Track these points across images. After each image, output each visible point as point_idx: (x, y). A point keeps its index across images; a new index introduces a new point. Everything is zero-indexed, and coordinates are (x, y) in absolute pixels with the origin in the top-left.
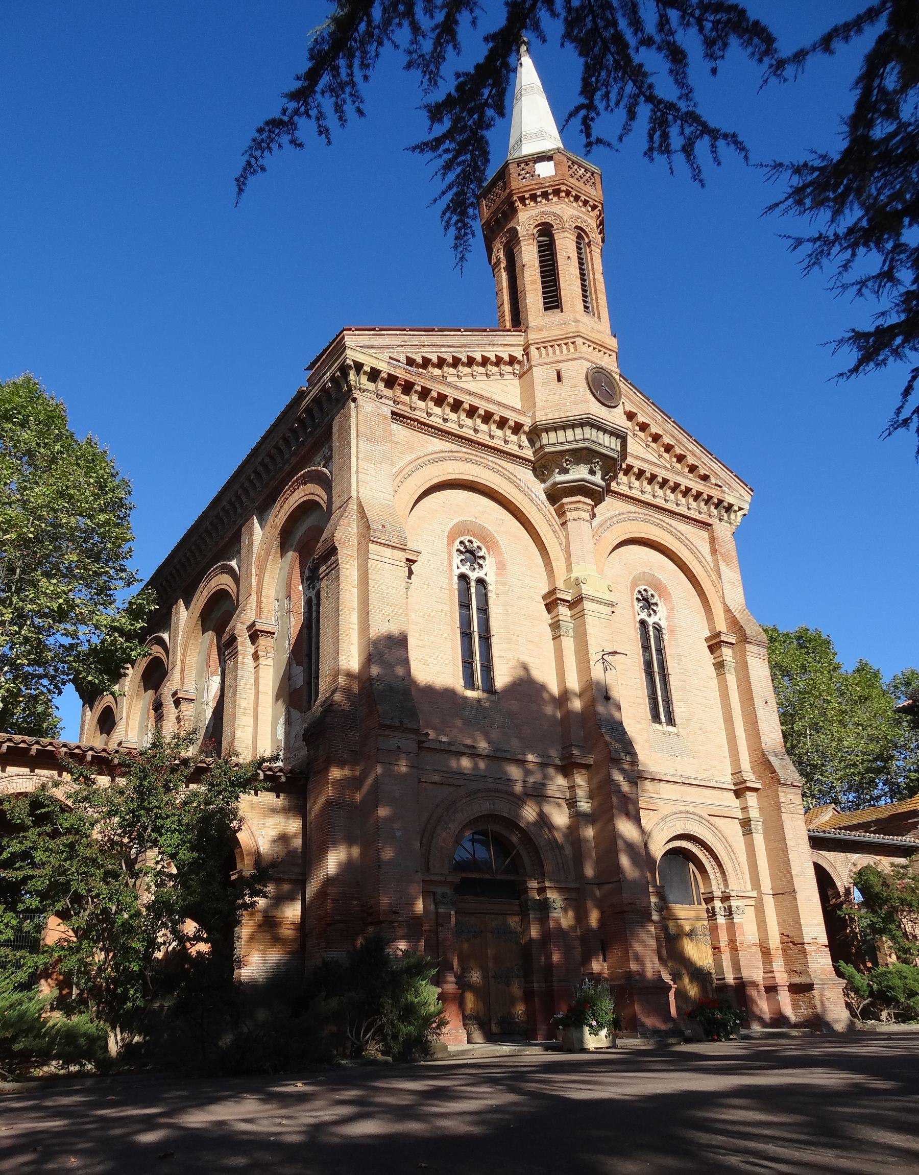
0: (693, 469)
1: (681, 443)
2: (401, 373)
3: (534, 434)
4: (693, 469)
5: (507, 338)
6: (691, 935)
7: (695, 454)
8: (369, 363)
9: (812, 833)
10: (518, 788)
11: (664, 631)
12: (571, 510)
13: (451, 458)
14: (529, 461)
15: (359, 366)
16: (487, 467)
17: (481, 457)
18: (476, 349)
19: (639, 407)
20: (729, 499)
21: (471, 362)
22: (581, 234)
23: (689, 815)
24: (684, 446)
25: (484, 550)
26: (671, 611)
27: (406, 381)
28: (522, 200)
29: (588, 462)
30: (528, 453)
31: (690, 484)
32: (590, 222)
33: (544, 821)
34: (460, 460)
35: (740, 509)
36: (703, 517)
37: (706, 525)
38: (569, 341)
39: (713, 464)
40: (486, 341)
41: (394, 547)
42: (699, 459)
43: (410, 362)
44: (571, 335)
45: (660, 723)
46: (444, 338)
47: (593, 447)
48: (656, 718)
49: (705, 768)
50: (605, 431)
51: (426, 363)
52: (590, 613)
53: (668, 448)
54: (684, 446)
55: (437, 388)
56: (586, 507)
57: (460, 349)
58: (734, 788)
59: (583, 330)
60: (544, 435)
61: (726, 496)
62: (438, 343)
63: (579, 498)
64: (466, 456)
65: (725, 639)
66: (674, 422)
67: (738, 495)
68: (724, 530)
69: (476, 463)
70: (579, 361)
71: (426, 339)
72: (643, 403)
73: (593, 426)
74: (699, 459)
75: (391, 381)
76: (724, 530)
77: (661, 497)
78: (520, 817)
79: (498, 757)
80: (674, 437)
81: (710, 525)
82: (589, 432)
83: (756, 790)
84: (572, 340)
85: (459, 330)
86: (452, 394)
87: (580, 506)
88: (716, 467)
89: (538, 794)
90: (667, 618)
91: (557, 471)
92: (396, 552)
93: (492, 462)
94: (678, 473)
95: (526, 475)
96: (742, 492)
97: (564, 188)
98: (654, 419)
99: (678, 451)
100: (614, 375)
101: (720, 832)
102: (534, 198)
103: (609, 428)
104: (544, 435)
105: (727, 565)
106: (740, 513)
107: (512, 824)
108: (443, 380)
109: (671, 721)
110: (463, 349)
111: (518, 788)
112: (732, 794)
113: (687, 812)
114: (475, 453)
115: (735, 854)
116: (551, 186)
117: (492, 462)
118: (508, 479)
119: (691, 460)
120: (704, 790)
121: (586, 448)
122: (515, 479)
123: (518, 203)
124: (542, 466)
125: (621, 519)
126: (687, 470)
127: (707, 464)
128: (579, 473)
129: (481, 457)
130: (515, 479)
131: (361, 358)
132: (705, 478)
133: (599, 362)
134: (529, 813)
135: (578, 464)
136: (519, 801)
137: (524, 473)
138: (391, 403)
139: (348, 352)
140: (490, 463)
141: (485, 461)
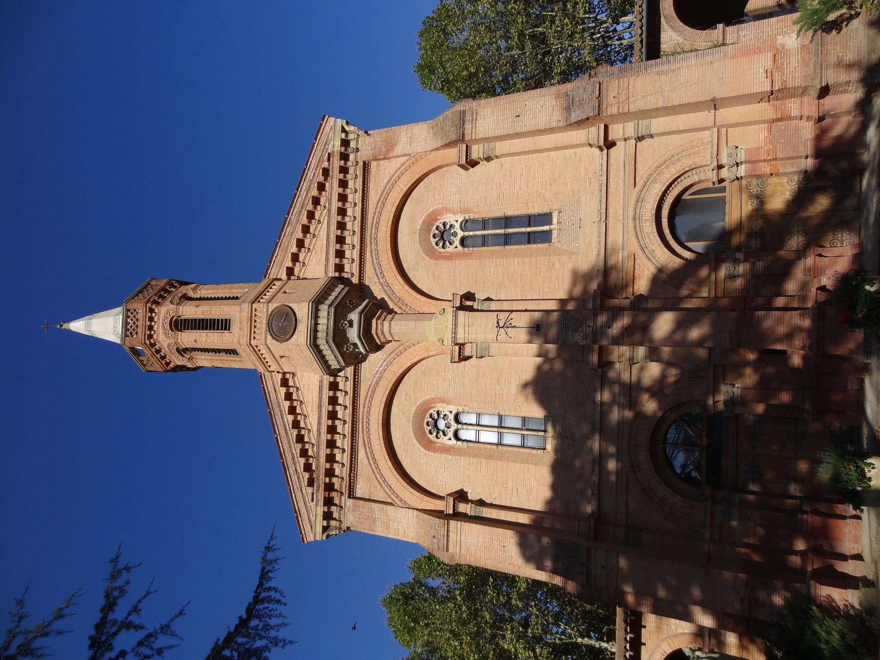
0: (321, 187)
2: (321, 495)
3: (334, 373)
4: (321, 187)
6: (761, 199)
7: (307, 189)
8: (320, 523)
9: (644, 58)
10: (628, 414)
11: (467, 218)
12: (385, 337)
13: (368, 446)
15: (325, 529)
16: (369, 412)
19: (286, 252)
20: (336, 146)
22: (179, 325)
23: (637, 216)
24: (305, 200)
25: (431, 411)
26: (447, 210)
27: (325, 491)
28: (168, 364)
29: (344, 332)
30: (350, 370)
31: (336, 183)
32: (165, 311)
33: (657, 390)
34: (369, 437)
35: (343, 130)
36: (360, 172)
37: (366, 166)
39: (312, 166)
40: (277, 411)
41: (448, 531)
42: (311, 181)
43: (311, 483)
45: (550, 231)
46: (286, 452)
48: (545, 237)
49: (588, 184)
50: (316, 324)
51: (308, 468)
52: (467, 336)
54: (305, 200)
55: (324, 451)
56: (380, 327)
58: (605, 151)
59: (245, 340)
60: (332, 367)
61: (336, 149)
63: (374, 332)
65: (464, 158)
67: (332, 131)
68: (365, 145)
69: (368, 422)
71: (291, 469)
73: (315, 338)
74: (311, 181)
75: (328, 502)
76: (365, 145)
78: (654, 416)
79: (601, 427)
80: (300, 212)
81: (364, 162)
82: (321, 342)
83: (606, 127)
86: (325, 437)
87: (379, 332)
88: (313, 162)
89: (631, 392)
90: (454, 213)
92: (451, 529)
94: (330, 201)
95: (365, 366)
96: (327, 129)
100: (270, 310)
101: (651, 175)
103: (313, 323)
105: (396, 145)
106: (347, 128)
107: (659, 424)
108: (317, 458)
109: (545, 218)
111: (628, 414)
112: (612, 150)
113: (634, 219)
115: (673, 156)
119: (314, 192)
120: (610, 190)
121: (334, 340)
123: (171, 365)
124: (355, 360)
126: (324, 193)
127: (313, 175)
131: (319, 529)
132: (326, 172)
134: (650, 406)
136: (640, 416)
138: (343, 498)
139: (318, 538)
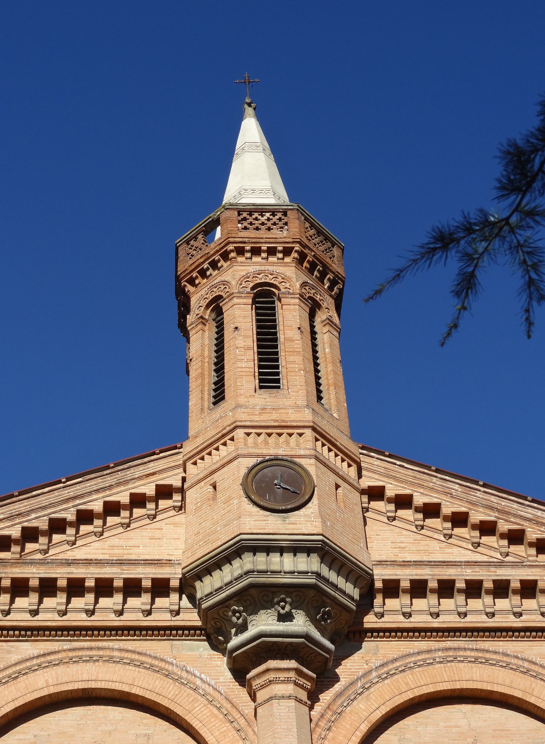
1: (508, 513)
5: (152, 464)
12: (263, 687)
13: (44, 662)
14: (195, 628)
16: (110, 660)
17: (99, 649)
18: (94, 497)
19: (413, 484)
21: (85, 517)
29: (268, 605)
30: (191, 618)
34: (61, 662)
38: (285, 431)
40: (110, 480)
44: (228, 429)
46: (33, 501)
47: (262, 579)
50: (281, 550)
53: (487, 528)
56: (282, 676)
57: (64, 506)
59: (244, 417)
60: (198, 584)
62: (23, 510)
63: (272, 664)
64: (71, 654)
66: (484, 486)
69: (91, 659)
70: (235, 462)
72: (419, 475)
73: (255, 549)
77: (477, 611)
80: (491, 508)
82: (248, 561)
84: (230, 436)
85: (60, 482)
87: (271, 676)
91: (233, 631)
93: (120, 650)
95: (203, 648)
97: (231, 247)
98: (446, 493)
99: (503, 527)
100: (303, 462)
102: (203, 274)
104: (198, 584)
110: (70, 504)
114: (93, 644)
116: (217, 251)
117: (120, 650)
118: (150, 668)
121: (251, 586)
122: (162, 665)
124: (214, 629)
125: (387, 671)
128: (264, 623)
129: (99, 649)
130: (162, 665)
133: (265, 452)
135: (255, 612)
137: (191, 649)
140: (116, 654)
141: (108, 653)
